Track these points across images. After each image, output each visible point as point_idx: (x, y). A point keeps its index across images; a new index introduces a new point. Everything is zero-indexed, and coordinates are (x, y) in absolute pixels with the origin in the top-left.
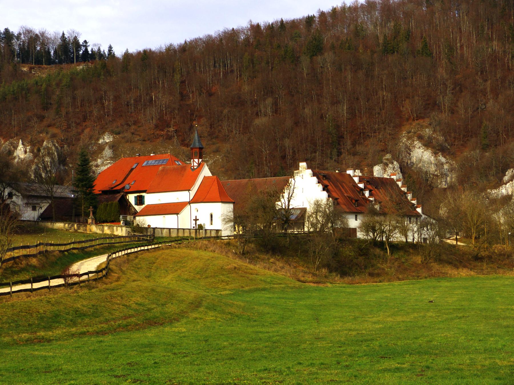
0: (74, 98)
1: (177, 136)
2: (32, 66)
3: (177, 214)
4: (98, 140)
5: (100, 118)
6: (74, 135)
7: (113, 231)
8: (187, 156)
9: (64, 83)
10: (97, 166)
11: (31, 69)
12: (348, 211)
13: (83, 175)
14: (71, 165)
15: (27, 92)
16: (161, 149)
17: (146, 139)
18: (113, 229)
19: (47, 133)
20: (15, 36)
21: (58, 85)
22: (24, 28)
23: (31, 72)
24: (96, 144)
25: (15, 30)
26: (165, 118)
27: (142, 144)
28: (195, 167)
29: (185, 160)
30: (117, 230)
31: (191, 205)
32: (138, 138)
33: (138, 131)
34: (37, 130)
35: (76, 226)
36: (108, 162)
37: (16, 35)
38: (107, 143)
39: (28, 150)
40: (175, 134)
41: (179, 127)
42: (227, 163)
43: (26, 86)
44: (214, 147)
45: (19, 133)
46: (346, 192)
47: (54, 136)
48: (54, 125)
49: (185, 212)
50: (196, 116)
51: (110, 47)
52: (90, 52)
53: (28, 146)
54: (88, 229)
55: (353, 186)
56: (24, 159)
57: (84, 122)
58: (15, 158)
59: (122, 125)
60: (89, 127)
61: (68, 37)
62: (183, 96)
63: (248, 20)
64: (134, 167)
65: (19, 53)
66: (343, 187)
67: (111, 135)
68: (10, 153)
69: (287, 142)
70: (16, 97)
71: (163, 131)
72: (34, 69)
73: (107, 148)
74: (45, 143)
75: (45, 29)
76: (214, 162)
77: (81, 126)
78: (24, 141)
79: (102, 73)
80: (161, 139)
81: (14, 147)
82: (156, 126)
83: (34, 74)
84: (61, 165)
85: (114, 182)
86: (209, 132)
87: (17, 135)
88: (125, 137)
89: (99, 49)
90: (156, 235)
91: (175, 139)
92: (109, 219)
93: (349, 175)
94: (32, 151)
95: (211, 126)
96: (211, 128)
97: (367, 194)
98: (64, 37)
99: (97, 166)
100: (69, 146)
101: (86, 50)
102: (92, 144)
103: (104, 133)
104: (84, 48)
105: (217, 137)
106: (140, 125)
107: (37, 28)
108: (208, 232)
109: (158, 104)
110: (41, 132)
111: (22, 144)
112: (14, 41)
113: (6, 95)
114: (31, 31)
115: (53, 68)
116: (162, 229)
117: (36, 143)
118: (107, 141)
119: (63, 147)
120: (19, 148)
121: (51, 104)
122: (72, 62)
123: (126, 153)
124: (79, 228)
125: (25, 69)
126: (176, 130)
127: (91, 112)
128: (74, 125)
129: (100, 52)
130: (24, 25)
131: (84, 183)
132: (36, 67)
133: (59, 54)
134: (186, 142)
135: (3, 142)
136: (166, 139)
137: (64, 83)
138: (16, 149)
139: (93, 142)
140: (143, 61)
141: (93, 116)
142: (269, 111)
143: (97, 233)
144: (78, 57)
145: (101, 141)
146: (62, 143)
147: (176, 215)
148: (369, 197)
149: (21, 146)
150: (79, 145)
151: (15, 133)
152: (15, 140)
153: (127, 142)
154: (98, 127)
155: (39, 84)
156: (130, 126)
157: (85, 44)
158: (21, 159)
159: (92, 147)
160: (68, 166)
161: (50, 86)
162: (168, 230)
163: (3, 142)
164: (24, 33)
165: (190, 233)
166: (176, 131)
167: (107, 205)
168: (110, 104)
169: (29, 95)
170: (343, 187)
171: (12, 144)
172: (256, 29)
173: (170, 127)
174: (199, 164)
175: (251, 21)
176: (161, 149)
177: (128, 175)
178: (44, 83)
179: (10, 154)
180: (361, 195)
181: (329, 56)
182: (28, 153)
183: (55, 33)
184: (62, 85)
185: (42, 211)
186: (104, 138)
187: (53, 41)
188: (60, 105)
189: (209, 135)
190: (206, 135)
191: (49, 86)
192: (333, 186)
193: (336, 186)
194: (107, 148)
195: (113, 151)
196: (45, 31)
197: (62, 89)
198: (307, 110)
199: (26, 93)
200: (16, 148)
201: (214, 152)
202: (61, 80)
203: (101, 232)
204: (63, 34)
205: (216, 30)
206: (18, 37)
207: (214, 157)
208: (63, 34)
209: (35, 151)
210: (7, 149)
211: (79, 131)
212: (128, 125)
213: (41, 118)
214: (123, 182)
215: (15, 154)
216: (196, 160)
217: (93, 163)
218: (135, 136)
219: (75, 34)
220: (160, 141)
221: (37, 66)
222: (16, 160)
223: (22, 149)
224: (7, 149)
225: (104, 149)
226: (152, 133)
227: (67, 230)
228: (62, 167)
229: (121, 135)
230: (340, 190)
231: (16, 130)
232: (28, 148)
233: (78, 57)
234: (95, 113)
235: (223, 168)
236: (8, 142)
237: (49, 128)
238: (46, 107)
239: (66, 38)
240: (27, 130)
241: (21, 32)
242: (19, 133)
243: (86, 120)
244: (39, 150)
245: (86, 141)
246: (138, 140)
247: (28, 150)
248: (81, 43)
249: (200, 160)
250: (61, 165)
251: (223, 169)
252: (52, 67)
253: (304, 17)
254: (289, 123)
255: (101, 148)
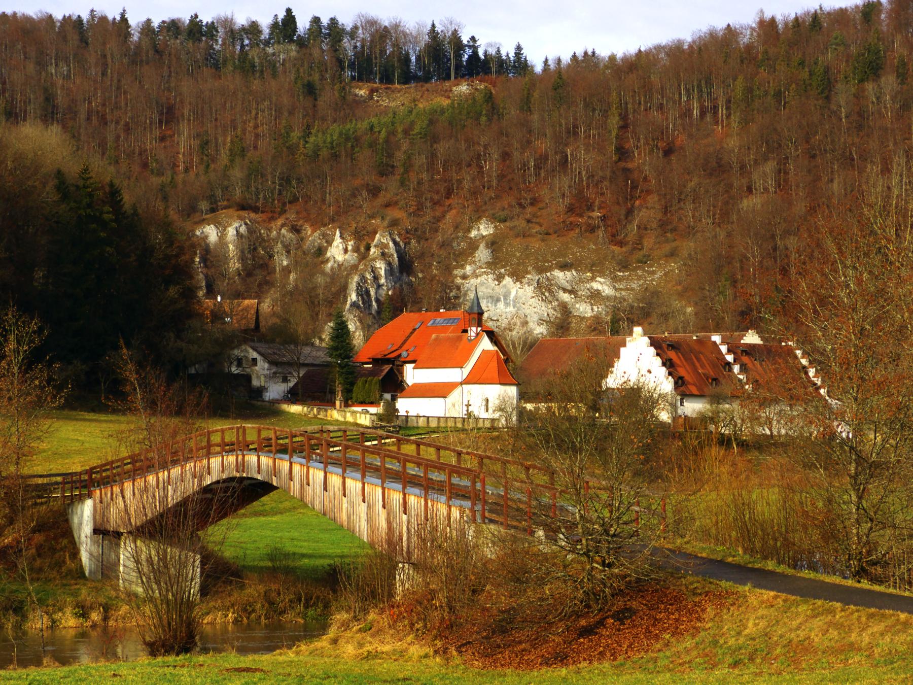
0: (433, 156)
1: (604, 226)
2: (375, 85)
3: (445, 397)
4: (469, 231)
5: (474, 193)
6: (430, 222)
7: (356, 418)
8: (618, 264)
9: (417, 129)
10: (464, 277)
11: (372, 91)
12: (697, 393)
13: (338, 342)
14: (420, 275)
15: (354, 144)
16: (575, 250)
17: (551, 231)
18: (356, 416)
19: (383, 218)
20: (347, 33)
21: (406, 132)
22: (363, 16)
23: (372, 98)
24: (465, 237)
25: (347, 21)
26: (587, 194)
27: (543, 240)
28: (472, 338)
29: (614, 269)
30: (360, 417)
31: (463, 386)
32: (537, 228)
33: (537, 217)
34: (366, 213)
35: (315, 409)
36: (483, 270)
37: (348, 29)
38: (483, 237)
39: (350, 248)
40: (601, 224)
41: (610, 211)
42: (687, 275)
43: (353, 133)
44: (667, 248)
45: (336, 217)
46: (703, 367)
47: (394, 223)
48: (396, 203)
49: (455, 396)
50: (642, 191)
51: (519, 48)
52: (483, 57)
53: (350, 241)
54: (328, 415)
55: (718, 359)
56: (342, 264)
57: (448, 198)
58: (328, 260)
59: (510, 206)
60: (455, 208)
61: (442, 31)
62: (623, 153)
63: (757, 9)
64: (417, 327)
65: (355, 61)
66: (699, 360)
67: (492, 223)
68: (321, 251)
69: (792, 242)
70: (335, 153)
71: (581, 216)
72: (377, 91)
73: (482, 246)
74: (378, 236)
75: (399, 18)
76: (665, 274)
77: (441, 205)
78: (343, 232)
79: (484, 112)
80: (577, 231)
81: (327, 242)
82: (571, 209)
83: (378, 101)
84: (405, 274)
85: (389, 347)
86: (660, 220)
87: (333, 220)
88: (515, 227)
89: (498, 51)
90: (409, 424)
91: (600, 233)
92: (367, 400)
93: (715, 342)
94: (356, 249)
95: (666, 210)
96: (665, 213)
97: (736, 369)
98: (434, 31)
99: (464, 277)
100: (419, 242)
101: (475, 53)
102: (458, 238)
103: (479, 218)
104: (471, 51)
105: (674, 230)
106: (541, 205)
107: (385, 18)
108: (481, 421)
109: (576, 168)
110: (372, 217)
111: (341, 236)
112: (346, 43)
113: (319, 150)
114: (376, 22)
115: (412, 90)
116: (418, 417)
117: (364, 235)
118: (484, 234)
119: (409, 243)
120: (335, 244)
121: (393, 167)
122: (448, 77)
123: (515, 256)
124: (318, 413)
125: (362, 92)
126: (604, 216)
127: (460, 182)
128: (428, 204)
129: (501, 56)
130: (363, 13)
131: (339, 352)
132: (381, 89)
133: (424, 62)
134: (619, 238)
135: (309, 233)
136: (586, 231)
137: (417, 129)
138: (331, 246)
139: (460, 234)
140: (555, 89)
141: (462, 189)
142: (771, 183)
143: (338, 420)
144: (458, 66)
145: (473, 233)
146: (407, 235)
147: (442, 399)
148: (738, 374)
149: (338, 241)
150: (436, 240)
151: (330, 217)
152: (329, 229)
153: (517, 236)
154: (471, 208)
155: (376, 130)
156: (524, 208)
157: (471, 44)
158: (338, 262)
159: (459, 245)
160: (416, 276)
161: (394, 134)
162: (425, 419)
163: (309, 233)
164: (362, 27)
165: (455, 423)
166: (604, 218)
167: (366, 381)
168: (491, 166)
169: (356, 149)
170: (699, 360)
171: (324, 235)
172: (768, 26)
173: (593, 211)
174: (477, 334)
175: (762, 11)
176: (575, 250)
177: (408, 338)
178: (384, 129)
179: (321, 254)
180: (727, 370)
181: (889, 82)
182: (349, 253)
183: (418, 24)
184: (414, 133)
185: (291, 384)
186: (479, 227)
187: (416, 38)
188: (408, 166)
189: (661, 226)
190: (654, 226)
191: (392, 133)
192: (682, 359)
193: (688, 359)
194: (482, 246)
195: (492, 252)
196: (400, 22)
197: (413, 139)
198: (835, 185)
199: (352, 146)
200: (330, 243)
201: (666, 256)
202: (412, 123)
203: (343, 420)
204: (433, 26)
205: (695, 30)
206: (353, 34)
207: (666, 266)
208: (433, 26)
209: (362, 249)
210: (316, 244)
211: (438, 214)
212: (520, 205)
213: (375, 192)
214: (400, 347)
215: (329, 254)
216: (474, 329)
217: (458, 272)
218: (533, 225)
219: (453, 25)
220: (575, 235)
221: (383, 87)
222: (329, 265)
223: (340, 245)
224: (316, 244)
225: (477, 248)
226: (562, 220)
227: (305, 415)
228: (405, 278)
229: (508, 224)
230: (693, 364)
231: (331, 211)
232: (350, 243)
233: (458, 66)
234: (466, 185)
235: (680, 284)
236: (318, 232)
237: (389, 208)
238: (385, 170)
239: (438, 33)
240: (349, 213)
241: (359, 24)
242: (336, 217)
243: (451, 195)
244: (368, 248)
245: (449, 233)
246: (536, 233)
247: (350, 248)
248: (465, 42)
249: (479, 329)
250: (405, 274)
251: (679, 288)
252: (411, 87)
253: (857, 7)
254: (800, 207)
255: (473, 246)
